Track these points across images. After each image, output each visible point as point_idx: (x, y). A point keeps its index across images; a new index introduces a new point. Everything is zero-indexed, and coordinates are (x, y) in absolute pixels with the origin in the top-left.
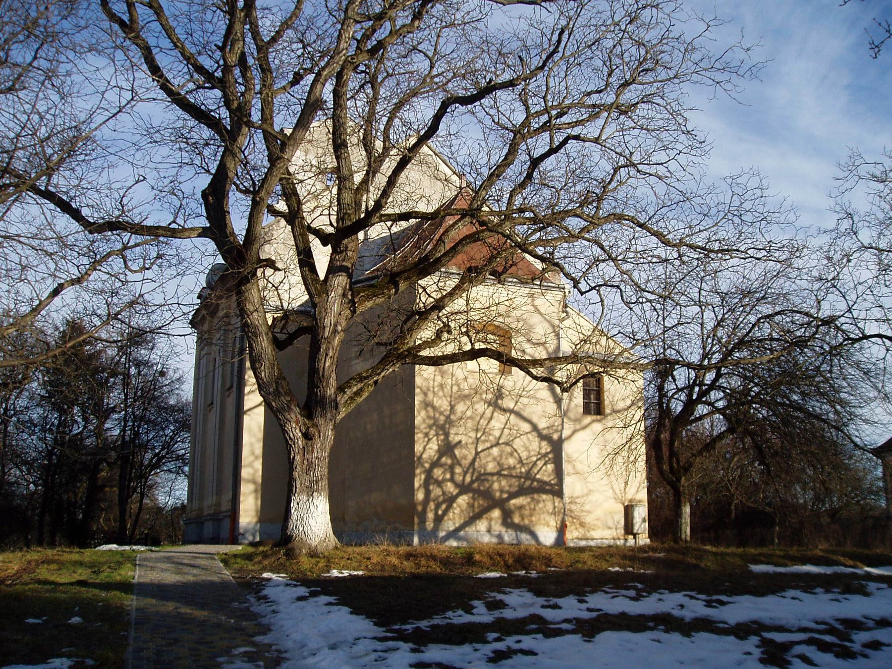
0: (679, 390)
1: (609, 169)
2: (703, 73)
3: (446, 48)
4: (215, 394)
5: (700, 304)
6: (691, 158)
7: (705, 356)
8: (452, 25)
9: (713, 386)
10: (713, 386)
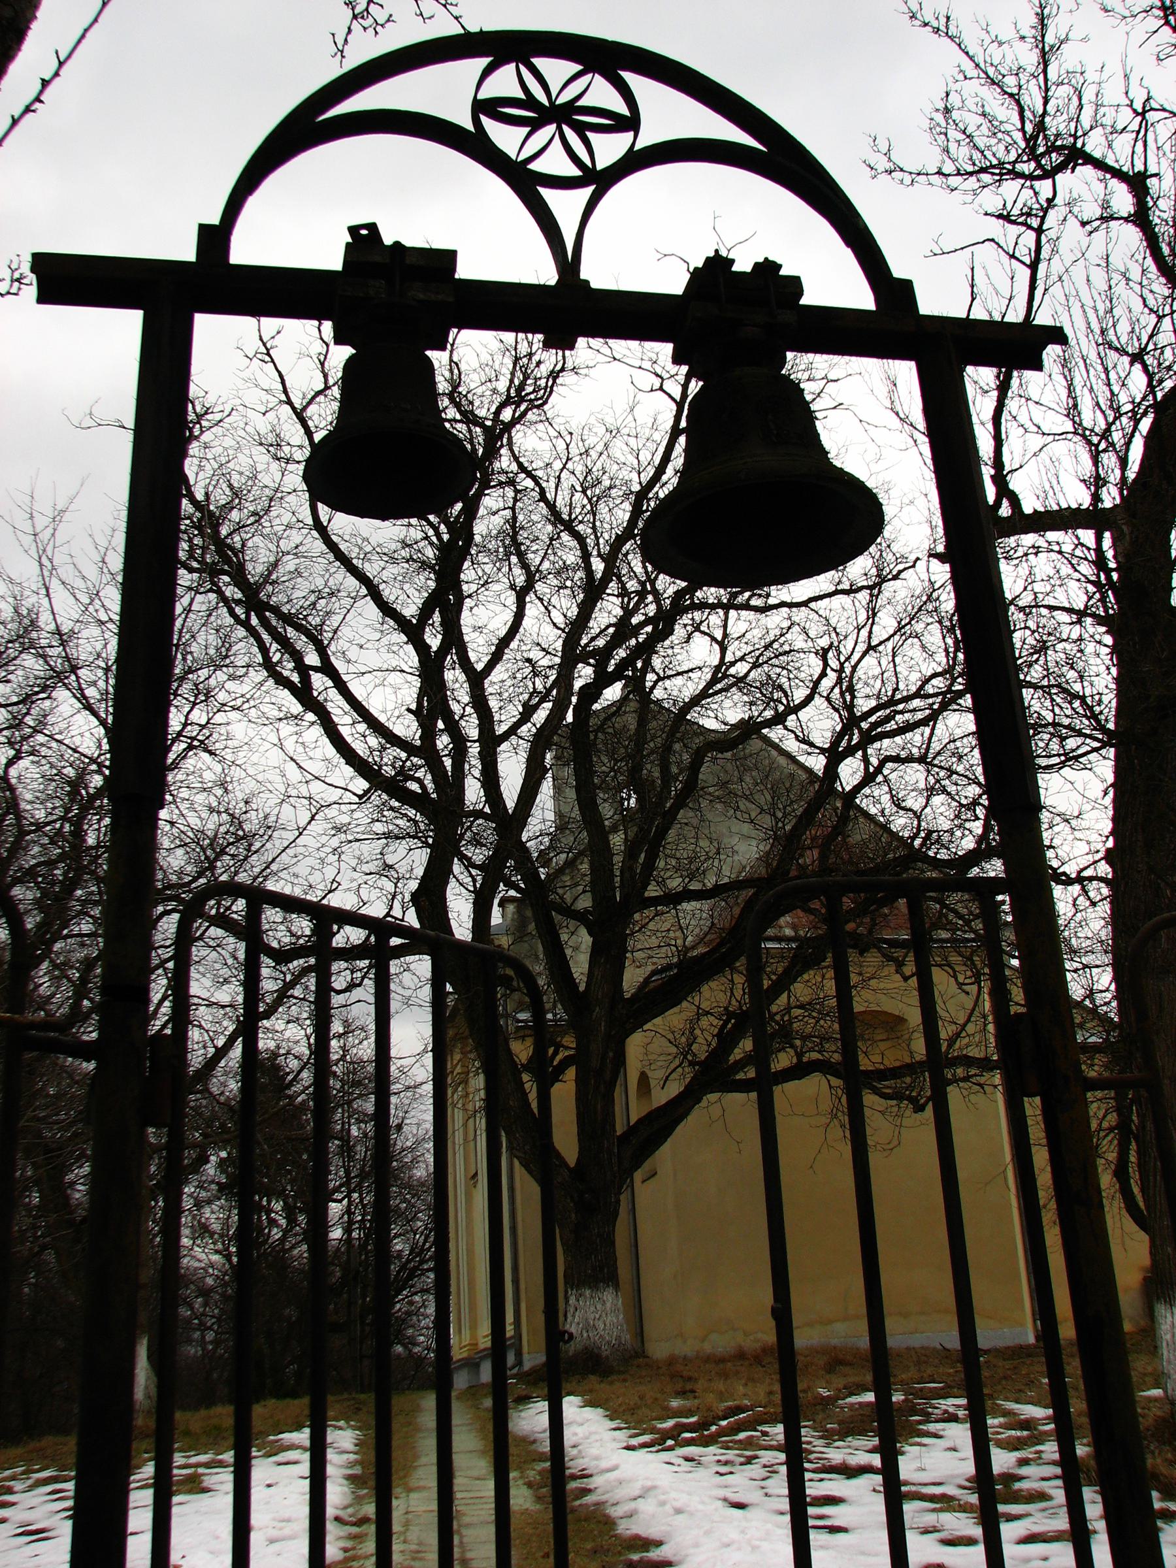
4: (479, 1157)
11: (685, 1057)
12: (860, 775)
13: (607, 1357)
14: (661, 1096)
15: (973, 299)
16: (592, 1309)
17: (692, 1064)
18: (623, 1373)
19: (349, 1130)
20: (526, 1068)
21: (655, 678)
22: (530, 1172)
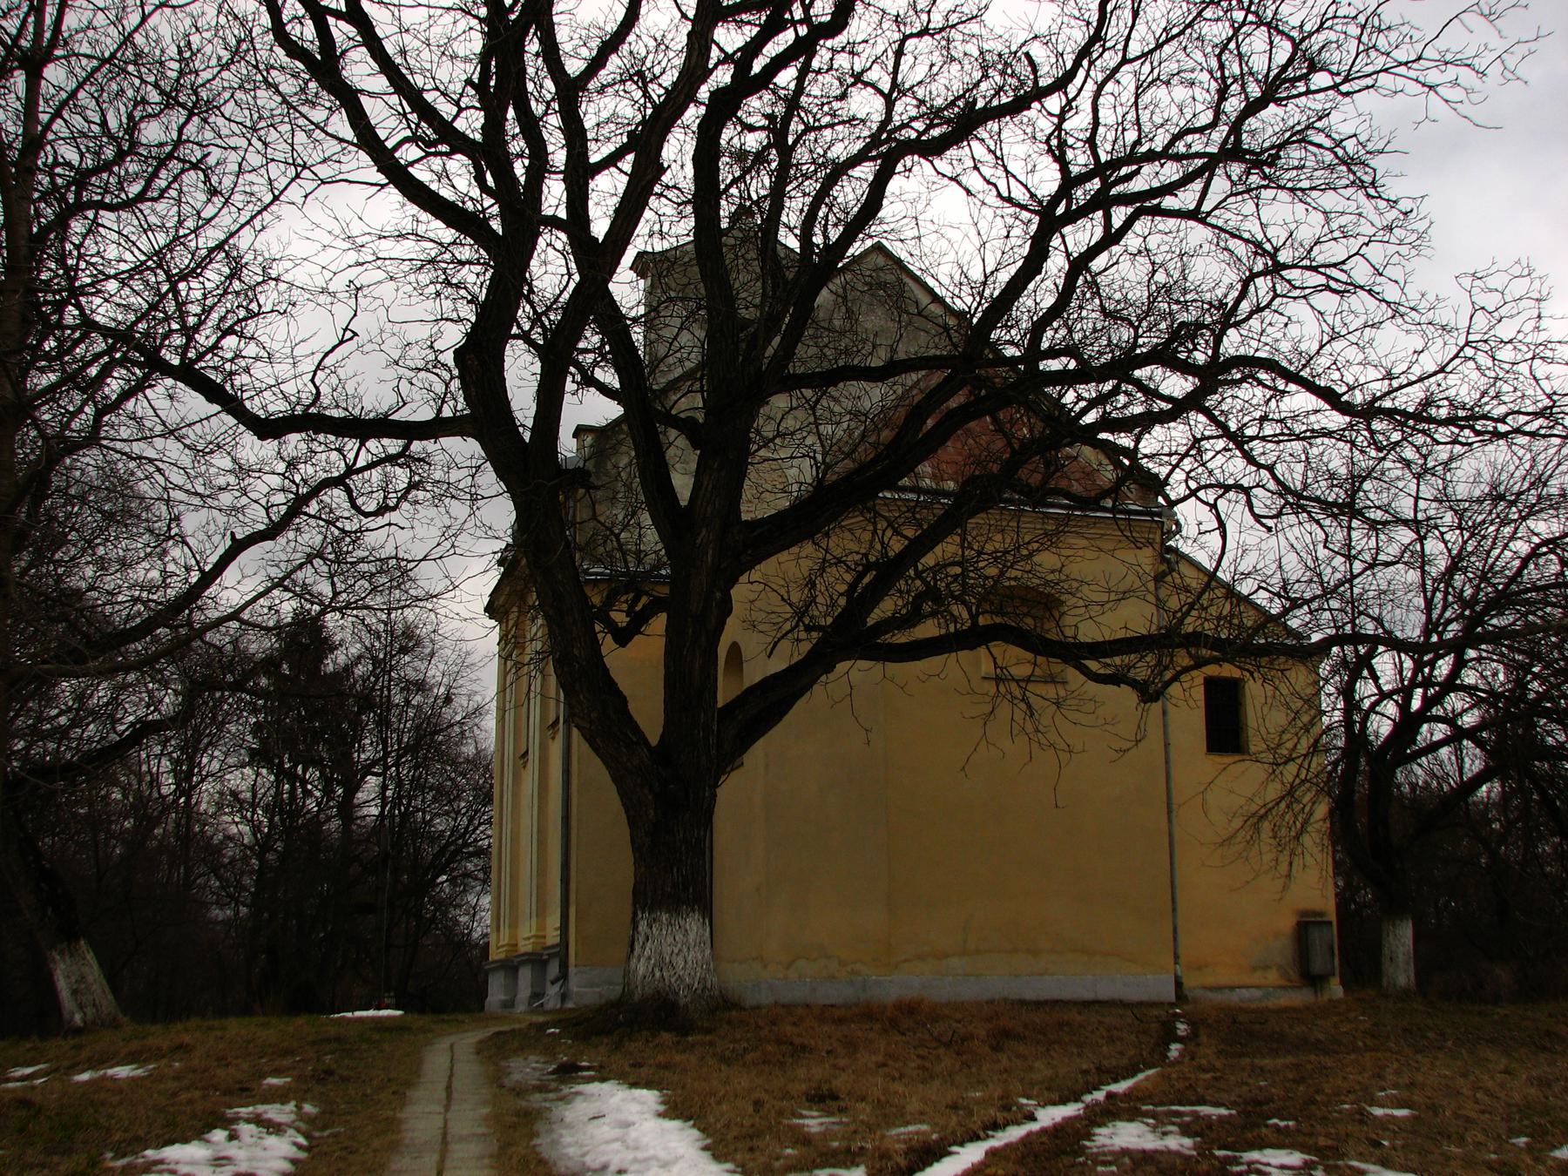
0: (1383, 696)
1: (1232, 277)
2: (1402, 70)
3: (912, 72)
4: (531, 734)
5: (1414, 524)
6: (1392, 249)
7: (1428, 630)
8: (924, 32)
9: (1451, 684)
10: (1451, 684)
11: (800, 620)
12: (1099, 233)
13: (686, 1005)
14: (758, 669)
15: (938, 173)
16: (670, 939)
17: (808, 629)
18: (709, 1031)
19: (389, 697)
20: (698, 103)
21: (801, 127)
22: (596, 749)
